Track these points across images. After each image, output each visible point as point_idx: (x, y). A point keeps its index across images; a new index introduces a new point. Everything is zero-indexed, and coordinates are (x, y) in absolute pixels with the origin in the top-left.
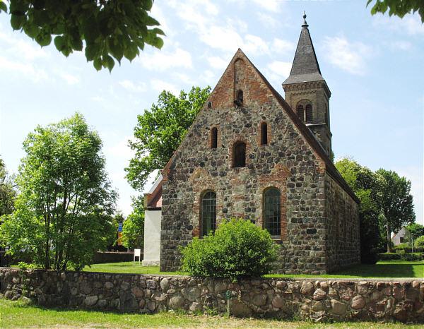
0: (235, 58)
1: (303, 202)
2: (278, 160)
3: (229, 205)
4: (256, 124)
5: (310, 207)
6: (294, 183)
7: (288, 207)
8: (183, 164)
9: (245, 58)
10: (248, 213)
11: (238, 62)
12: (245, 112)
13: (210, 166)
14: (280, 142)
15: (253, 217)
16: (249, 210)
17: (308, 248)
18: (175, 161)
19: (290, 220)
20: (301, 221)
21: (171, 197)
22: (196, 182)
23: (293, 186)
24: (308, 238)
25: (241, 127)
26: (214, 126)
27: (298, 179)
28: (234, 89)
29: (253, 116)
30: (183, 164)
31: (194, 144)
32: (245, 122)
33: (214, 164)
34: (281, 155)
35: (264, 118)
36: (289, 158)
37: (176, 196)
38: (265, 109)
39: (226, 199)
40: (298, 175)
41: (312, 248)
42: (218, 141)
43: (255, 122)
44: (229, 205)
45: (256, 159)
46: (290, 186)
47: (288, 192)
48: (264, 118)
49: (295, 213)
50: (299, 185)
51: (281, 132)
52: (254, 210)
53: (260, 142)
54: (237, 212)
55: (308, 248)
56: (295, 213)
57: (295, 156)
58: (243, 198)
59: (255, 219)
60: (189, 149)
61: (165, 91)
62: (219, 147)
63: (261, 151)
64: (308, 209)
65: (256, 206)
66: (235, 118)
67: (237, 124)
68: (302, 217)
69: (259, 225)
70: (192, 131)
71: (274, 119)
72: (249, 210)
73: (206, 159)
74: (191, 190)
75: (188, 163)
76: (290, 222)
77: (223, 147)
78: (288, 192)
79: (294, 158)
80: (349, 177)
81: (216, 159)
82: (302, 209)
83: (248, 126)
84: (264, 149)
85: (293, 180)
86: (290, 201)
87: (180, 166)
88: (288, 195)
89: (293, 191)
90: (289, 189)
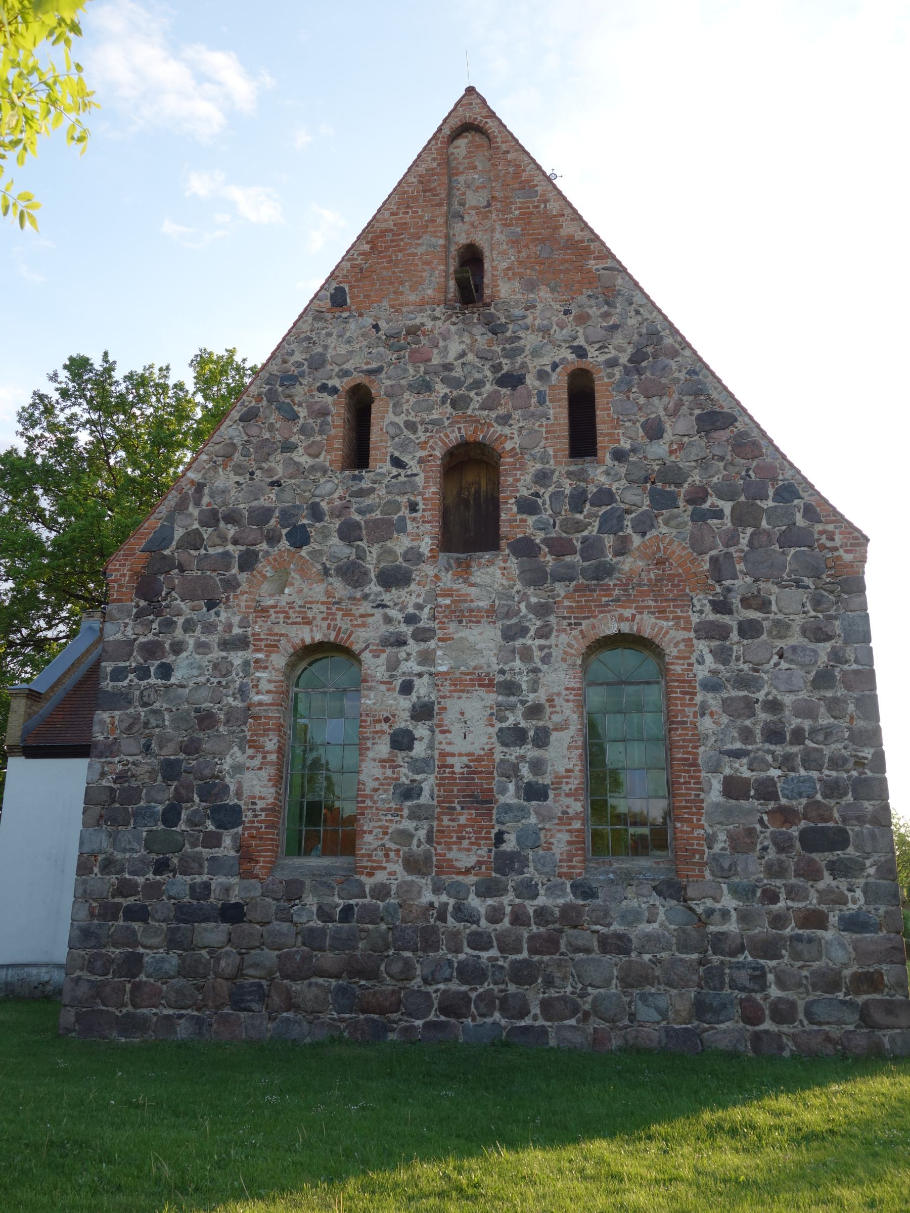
0: (455, 122)
1: (774, 706)
2: (643, 526)
3: (423, 712)
4: (542, 375)
5: (807, 724)
6: (726, 619)
7: (706, 724)
8: (207, 532)
9: (490, 123)
10: (516, 752)
11: (462, 142)
12: (496, 330)
13: (335, 540)
14: (659, 449)
15: (537, 766)
16: (516, 736)
17: (816, 920)
18: (171, 518)
19: (717, 785)
20: (767, 791)
21: (143, 673)
22: (265, 610)
23: (721, 632)
24: (811, 873)
25: (478, 385)
26: (359, 378)
27: (746, 603)
28: (447, 237)
29: (530, 340)
30: (207, 532)
31: (265, 450)
32: (496, 368)
33: (349, 533)
34: (661, 501)
35: (581, 352)
36: (699, 517)
37: (166, 671)
38: (583, 319)
39: (407, 688)
40: (741, 583)
41: (833, 919)
42: (374, 437)
43: (534, 365)
44: (423, 712)
45: (545, 516)
46: (709, 631)
47: (701, 662)
48: (581, 352)
49: (737, 754)
50: (749, 630)
51: (658, 407)
52: (542, 739)
53: (564, 444)
54: (460, 745)
55: (816, 920)
56: (737, 754)
57: (727, 507)
58: (486, 683)
59: (547, 780)
60: (239, 469)
61: (231, 352)
62: (381, 465)
63: (567, 486)
64: (798, 736)
65: (550, 720)
66: (454, 348)
67: (458, 373)
68: (774, 773)
69: (571, 896)
70: (259, 398)
71: (624, 359)
72: (516, 736)
73: (316, 513)
74: (242, 643)
75: (232, 531)
76: (715, 795)
77: (397, 463)
78: (701, 662)
79: (718, 514)
80: (111, 840)
81: (360, 512)
82: (774, 735)
83: (513, 380)
84: (580, 476)
85: (721, 607)
86: (713, 701)
87: (193, 541)
88: (702, 672)
89: (722, 655)
90: (702, 646)
